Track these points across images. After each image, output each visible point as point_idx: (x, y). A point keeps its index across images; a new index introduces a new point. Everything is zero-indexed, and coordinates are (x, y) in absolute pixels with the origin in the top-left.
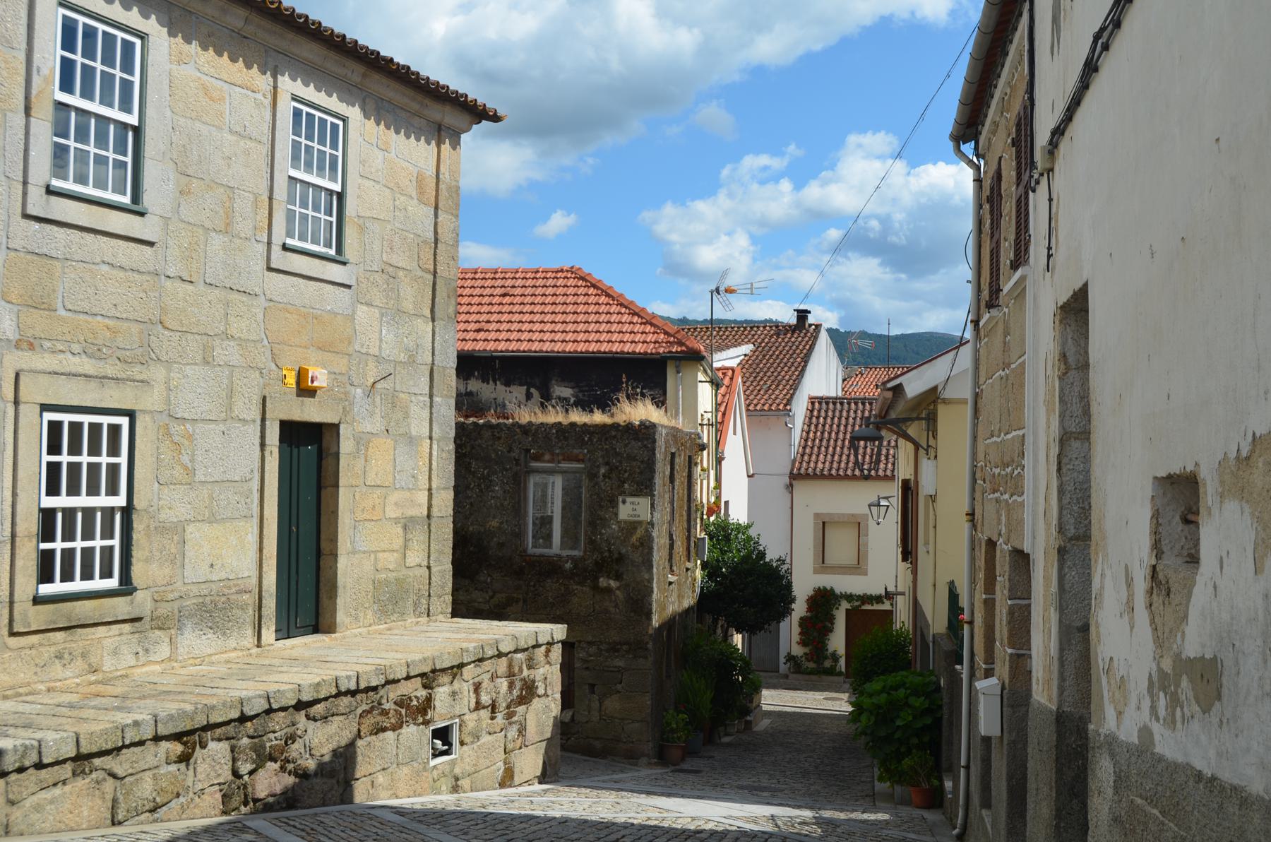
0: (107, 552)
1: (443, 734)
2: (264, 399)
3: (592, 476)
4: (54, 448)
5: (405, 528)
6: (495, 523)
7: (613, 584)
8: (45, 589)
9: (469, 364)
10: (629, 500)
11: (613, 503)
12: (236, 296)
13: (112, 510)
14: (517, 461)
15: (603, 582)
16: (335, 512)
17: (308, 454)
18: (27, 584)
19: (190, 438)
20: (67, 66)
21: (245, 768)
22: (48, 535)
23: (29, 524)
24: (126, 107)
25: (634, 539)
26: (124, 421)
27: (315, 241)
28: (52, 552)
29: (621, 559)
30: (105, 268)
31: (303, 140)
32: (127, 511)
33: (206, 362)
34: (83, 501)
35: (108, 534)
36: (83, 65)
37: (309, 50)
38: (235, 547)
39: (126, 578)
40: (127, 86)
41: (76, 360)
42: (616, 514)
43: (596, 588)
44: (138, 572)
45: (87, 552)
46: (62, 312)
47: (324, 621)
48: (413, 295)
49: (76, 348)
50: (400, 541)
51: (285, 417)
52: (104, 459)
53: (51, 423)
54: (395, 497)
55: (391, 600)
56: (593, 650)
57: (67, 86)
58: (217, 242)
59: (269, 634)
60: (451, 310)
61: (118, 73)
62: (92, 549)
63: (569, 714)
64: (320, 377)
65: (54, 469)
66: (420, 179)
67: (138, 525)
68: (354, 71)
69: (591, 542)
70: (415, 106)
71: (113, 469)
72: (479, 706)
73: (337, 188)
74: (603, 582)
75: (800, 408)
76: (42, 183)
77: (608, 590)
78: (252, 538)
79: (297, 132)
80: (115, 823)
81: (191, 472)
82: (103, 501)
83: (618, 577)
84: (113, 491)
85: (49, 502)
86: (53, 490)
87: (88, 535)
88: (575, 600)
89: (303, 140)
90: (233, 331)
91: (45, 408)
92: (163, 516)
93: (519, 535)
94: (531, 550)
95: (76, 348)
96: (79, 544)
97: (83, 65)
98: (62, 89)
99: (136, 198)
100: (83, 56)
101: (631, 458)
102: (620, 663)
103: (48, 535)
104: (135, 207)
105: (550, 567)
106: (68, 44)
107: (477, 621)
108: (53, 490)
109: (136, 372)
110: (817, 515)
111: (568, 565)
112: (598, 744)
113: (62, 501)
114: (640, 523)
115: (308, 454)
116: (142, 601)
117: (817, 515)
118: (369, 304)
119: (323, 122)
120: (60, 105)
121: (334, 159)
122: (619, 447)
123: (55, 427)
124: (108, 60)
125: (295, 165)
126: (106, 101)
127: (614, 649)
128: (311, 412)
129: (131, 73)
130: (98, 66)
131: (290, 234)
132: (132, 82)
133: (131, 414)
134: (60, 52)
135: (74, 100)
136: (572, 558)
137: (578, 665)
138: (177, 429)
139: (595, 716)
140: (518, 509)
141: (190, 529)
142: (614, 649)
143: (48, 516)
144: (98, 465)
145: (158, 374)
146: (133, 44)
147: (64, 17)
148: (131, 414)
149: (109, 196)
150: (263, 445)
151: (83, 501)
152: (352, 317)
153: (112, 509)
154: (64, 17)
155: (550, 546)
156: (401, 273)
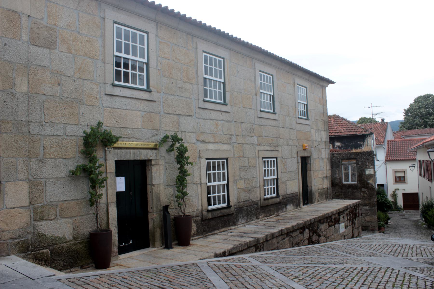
0: (224, 196)
2: (298, 152)
4: (209, 169)
5: (323, 179)
9: (332, 140)
10: (368, 169)
12: (291, 130)
13: (274, 179)
16: (311, 177)
19: (286, 162)
20: (206, 68)
22: (209, 193)
24: (220, 78)
26: (275, 159)
27: (268, 109)
30: (270, 127)
31: (263, 82)
32: (277, 179)
33: (287, 145)
34: (217, 183)
35: (224, 191)
36: (132, 45)
37: (299, 73)
40: (142, 50)
41: (267, 147)
42: (365, 173)
46: (264, 137)
48: (320, 125)
50: (322, 182)
51: (116, 159)
52: (221, 171)
53: (208, 162)
54: (320, 172)
57: (206, 74)
58: (287, 118)
60: (327, 128)
61: (218, 69)
62: (215, 196)
65: (209, 175)
66: (320, 99)
68: (307, 76)
71: (224, 174)
73: (272, 94)
75: (386, 143)
76: (111, 82)
78: (297, 184)
79: (261, 80)
81: (286, 169)
84: (224, 180)
85: (265, 178)
87: (219, 192)
89: (263, 82)
90: (291, 138)
92: (283, 180)
93: (341, 179)
94: (344, 183)
95: (267, 144)
96: (217, 195)
97: (132, 45)
98: (205, 74)
99: (307, 117)
100: (125, 40)
103: (209, 193)
104: (225, 104)
106: (206, 62)
107: (339, 200)
109: (277, 149)
110: (393, 170)
117: (393, 170)
118: (313, 129)
119: (211, 59)
120: (205, 78)
121: (220, 72)
123: (209, 163)
124: (216, 66)
125: (206, 74)
126: (216, 77)
128: (306, 155)
129: (221, 69)
130: (213, 67)
132: (116, 38)
133: (276, 158)
134: (204, 65)
135: (208, 77)
138: (284, 160)
141: (287, 182)
145: (280, 149)
146: (221, 61)
147: (205, 55)
148: (276, 158)
149: (218, 101)
150: (298, 163)
151: (217, 183)
152: (310, 132)
153: (224, 184)
154: (205, 55)
156: (318, 121)
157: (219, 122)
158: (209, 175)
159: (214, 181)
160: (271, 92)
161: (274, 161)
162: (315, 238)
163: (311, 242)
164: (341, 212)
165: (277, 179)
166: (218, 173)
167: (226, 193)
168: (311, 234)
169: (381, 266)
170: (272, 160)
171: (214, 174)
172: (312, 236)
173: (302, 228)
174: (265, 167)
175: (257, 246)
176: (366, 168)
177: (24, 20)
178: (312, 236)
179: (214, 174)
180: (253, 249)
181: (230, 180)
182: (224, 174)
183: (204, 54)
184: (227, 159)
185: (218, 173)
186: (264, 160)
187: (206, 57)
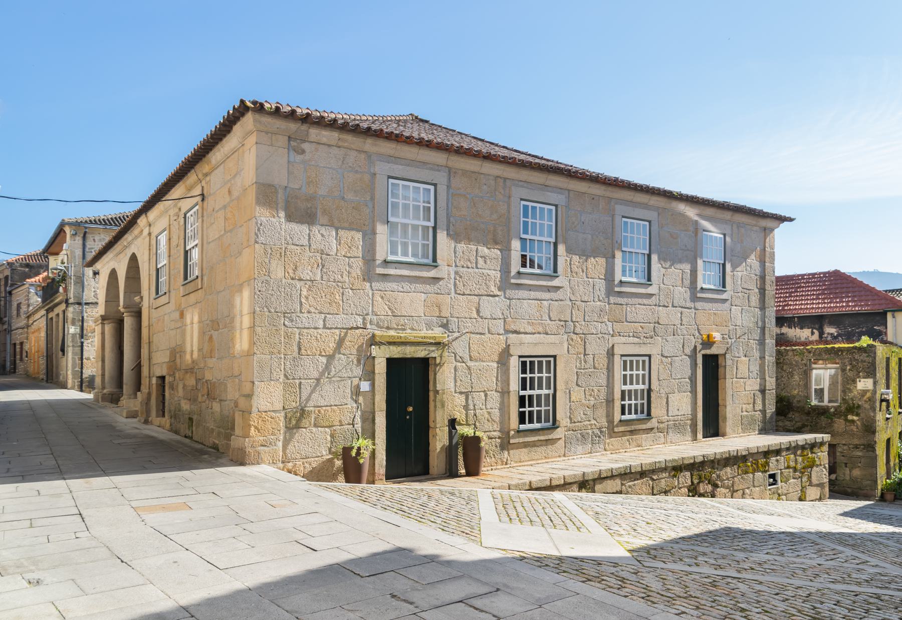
1: (773, 476)
3: (843, 370)
4: (625, 370)
6: (796, 392)
7: (855, 418)
8: (522, 427)
11: (854, 382)
14: (806, 365)
15: (850, 417)
16: (725, 389)
17: (712, 369)
18: (617, 416)
21: (696, 481)
23: (617, 395)
25: (865, 398)
28: (524, 412)
29: (859, 407)
35: (547, 405)
38: (680, 401)
39: (649, 414)
43: (846, 420)
44: (654, 412)
45: (630, 405)
47: (720, 431)
49: (631, 334)
51: (388, 356)
55: (746, 425)
56: (845, 447)
59: (700, 435)
63: (833, 477)
64: (717, 336)
67: (653, 395)
69: (843, 399)
70: (754, 222)
72: (788, 467)
74: (850, 417)
77: (853, 421)
80: (653, 494)
82: (544, 392)
83: (857, 415)
85: (624, 388)
86: (625, 384)
88: (836, 425)
91: (622, 356)
93: (808, 397)
101: (863, 361)
102: (860, 454)
103: (623, 399)
105: (822, 412)
106: (526, 215)
108: (625, 384)
111: (832, 410)
112: (849, 490)
113: (627, 388)
114: (868, 391)
115: (712, 369)
116: (653, 423)
122: (857, 356)
123: (625, 362)
127: (856, 447)
131: (624, 274)
136: (834, 407)
137: (838, 454)
139: (848, 478)
140: (807, 386)
142: (856, 447)
143: (623, 392)
144: (542, 377)
155: (823, 401)
157: (545, 302)
158: (625, 376)
159: (631, 383)
160: (644, 249)
161: (644, 362)
162: (702, 488)
163: (694, 491)
164: (773, 451)
165: (649, 391)
166: (530, 378)
167: (551, 408)
168: (696, 481)
169: (623, 592)
170: (644, 358)
171: (631, 376)
172: (698, 483)
173: (677, 469)
174: (625, 370)
175: (585, 484)
176: (859, 377)
177: (280, 191)
178: (698, 483)
179: (631, 376)
180: (575, 487)
181: (558, 387)
182: (644, 375)
183: (523, 203)
184: (555, 357)
185: (530, 378)
186: (624, 358)
187: (526, 208)
